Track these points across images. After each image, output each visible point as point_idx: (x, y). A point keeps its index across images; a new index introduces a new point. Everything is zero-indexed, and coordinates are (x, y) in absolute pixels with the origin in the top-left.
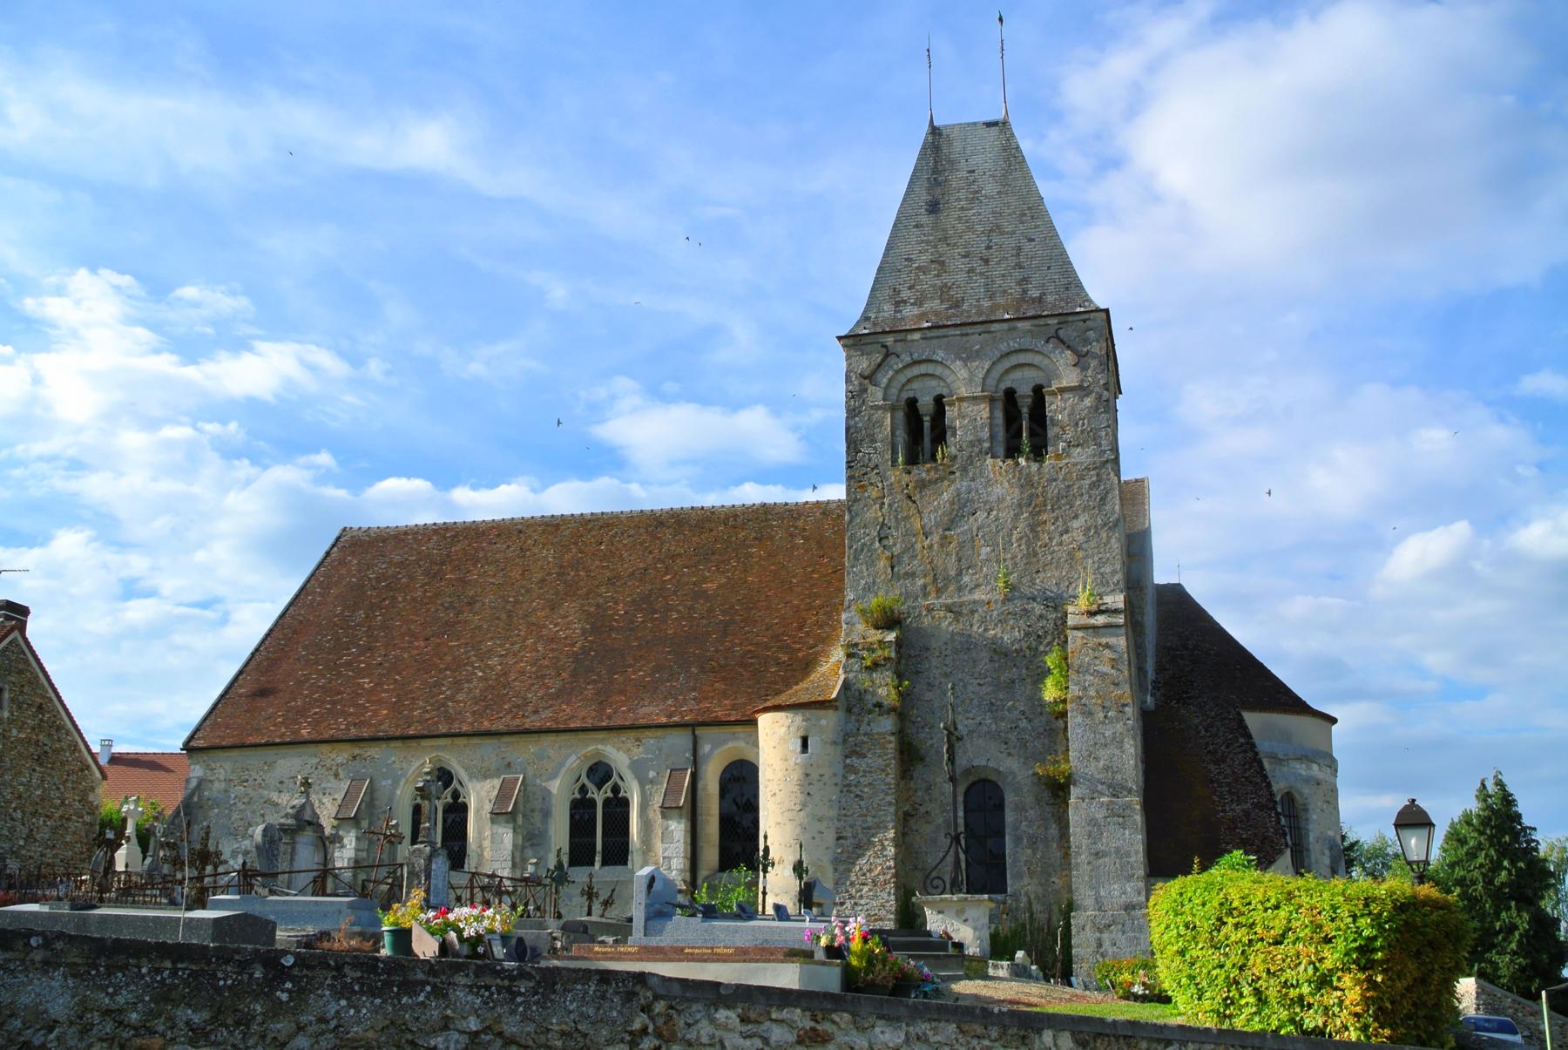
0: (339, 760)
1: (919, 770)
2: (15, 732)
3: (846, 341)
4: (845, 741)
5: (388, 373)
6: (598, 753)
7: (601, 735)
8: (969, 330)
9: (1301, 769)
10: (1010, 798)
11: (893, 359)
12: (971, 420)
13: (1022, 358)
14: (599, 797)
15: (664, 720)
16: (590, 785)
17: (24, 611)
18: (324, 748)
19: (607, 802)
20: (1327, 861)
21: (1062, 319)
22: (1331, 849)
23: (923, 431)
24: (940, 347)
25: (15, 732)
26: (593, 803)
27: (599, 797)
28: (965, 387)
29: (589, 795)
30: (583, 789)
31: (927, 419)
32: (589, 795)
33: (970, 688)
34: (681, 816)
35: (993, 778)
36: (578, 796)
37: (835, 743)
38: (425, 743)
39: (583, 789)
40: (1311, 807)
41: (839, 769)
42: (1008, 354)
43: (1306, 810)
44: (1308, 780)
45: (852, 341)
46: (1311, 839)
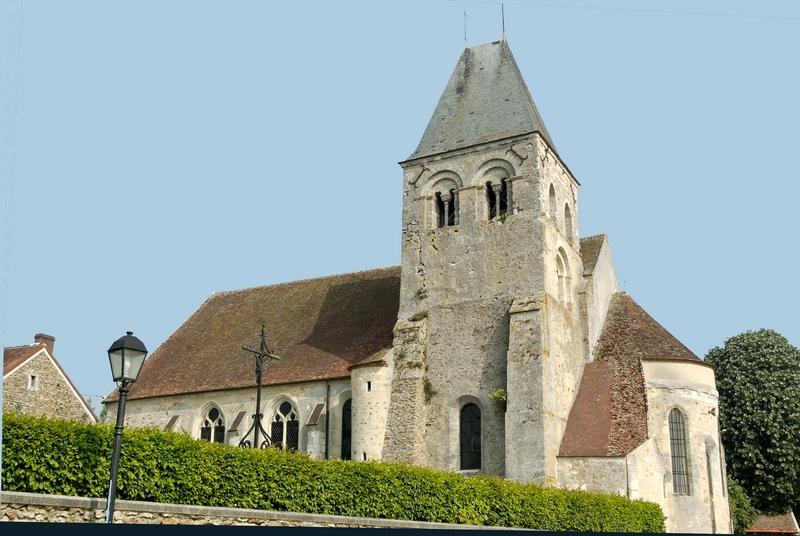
1: (434, 399)
2: (42, 398)
3: (404, 165)
6: (284, 397)
7: (284, 388)
9: (683, 394)
10: (484, 414)
11: (426, 173)
12: (473, 204)
13: (451, 176)
14: (285, 420)
15: (314, 378)
17: (52, 339)
18: (162, 400)
19: (288, 423)
21: (514, 139)
23: (447, 210)
25: (42, 398)
27: (285, 420)
28: (476, 176)
31: (446, 203)
34: (317, 429)
35: (475, 402)
38: (206, 395)
39: (278, 417)
42: (487, 162)
44: (688, 401)
45: (407, 164)
46: (691, 436)
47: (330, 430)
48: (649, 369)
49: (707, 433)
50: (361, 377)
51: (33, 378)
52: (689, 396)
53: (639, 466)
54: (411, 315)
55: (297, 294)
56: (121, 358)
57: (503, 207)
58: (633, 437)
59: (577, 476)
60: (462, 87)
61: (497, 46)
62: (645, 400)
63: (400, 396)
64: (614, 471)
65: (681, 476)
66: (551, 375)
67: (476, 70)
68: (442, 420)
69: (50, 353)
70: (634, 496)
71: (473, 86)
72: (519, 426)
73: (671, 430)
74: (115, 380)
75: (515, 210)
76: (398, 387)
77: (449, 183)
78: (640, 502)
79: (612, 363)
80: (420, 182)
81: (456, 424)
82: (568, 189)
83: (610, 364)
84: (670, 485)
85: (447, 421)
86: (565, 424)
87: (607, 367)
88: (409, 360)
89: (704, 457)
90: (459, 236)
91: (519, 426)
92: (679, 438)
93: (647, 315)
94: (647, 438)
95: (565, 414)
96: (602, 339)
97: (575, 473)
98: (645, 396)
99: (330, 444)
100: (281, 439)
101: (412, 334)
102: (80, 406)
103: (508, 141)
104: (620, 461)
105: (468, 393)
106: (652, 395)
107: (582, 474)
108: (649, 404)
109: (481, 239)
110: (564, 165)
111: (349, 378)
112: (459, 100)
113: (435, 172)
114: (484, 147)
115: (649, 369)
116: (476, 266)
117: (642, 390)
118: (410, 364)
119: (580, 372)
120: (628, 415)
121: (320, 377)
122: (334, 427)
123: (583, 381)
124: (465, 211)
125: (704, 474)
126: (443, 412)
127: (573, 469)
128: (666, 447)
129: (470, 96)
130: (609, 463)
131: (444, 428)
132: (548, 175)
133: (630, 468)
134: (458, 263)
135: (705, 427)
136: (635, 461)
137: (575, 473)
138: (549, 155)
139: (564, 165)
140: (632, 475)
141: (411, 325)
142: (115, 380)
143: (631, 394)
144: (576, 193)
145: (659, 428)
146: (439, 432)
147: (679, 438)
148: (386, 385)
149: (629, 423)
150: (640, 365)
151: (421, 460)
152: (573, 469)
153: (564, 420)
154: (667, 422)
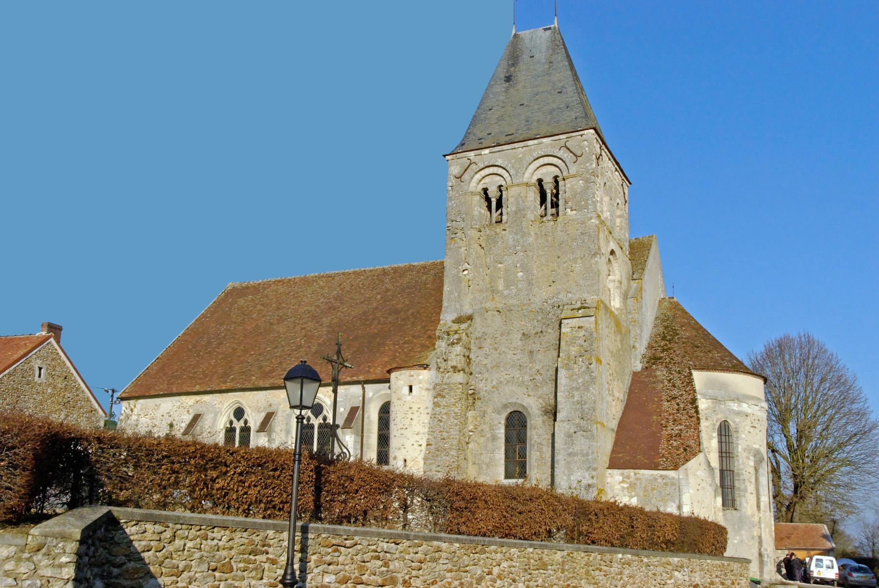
0: (190, 403)
4: (434, 388)
5: (617, 309)
8: (516, 145)
9: (734, 406)
14: (238, 425)
15: (349, 379)
16: (235, 420)
19: (320, 426)
20: (752, 463)
22: (755, 456)
24: (500, 157)
26: (312, 427)
27: (238, 425)
29: (311, 422)
30: (231, 423)
32: (311, 422)
33: (509, 356)
36: (229, 426)
37: (428, 389)
39: (231, 423)
40: (740, 430)
41: (430, 405)
43: (737, 432)
44: (738, 413)
47: (365, 434)
48: (699, 377)
49: (756, 446)
50: (400, 379)
51: (40, 369)
52: (740, 409)
53: (691, 480)
54: (454, 316)
55: (322, 288)
56: (299, 386)
57: (555, 205)
58: (685, 450)
59: (628, 488)
60: (511, 76)
61: (548, 33)
62: (697, 412)
63: (443, 402)
64: (666, 484)
65: (727, 487)
66: (602, 384)
67: (526, 57)
68: (486, 427)
69: (58, 342)
70: (686, 511)
71: (522, 74)
72: (569, 436)
73: (720, 442)
74: (292, 407)
75: (569, 210)
76: (439, 392)
77: (498, 178)
78: (650, 512)
79: (661, 373)
80: (466, 177)
81: (501, 432)
82: (620, 190)
83: (658, 373)
84: (719, 500)
85: (492, 428)
86: (614, 435)
87: (656, 376)
88: (454, 364)
89: (752, 471)
90: (507, 235)
91: (569, 436)
92: (726, 454)
93: (697, 323)
94: (700, 451)
95: (614, 424)
96: (650, 347)
97: (626, 486)
98: (697, 407)
99: (365, 449)
100: (312, 444)
101: (456, 336)
102: (89, 400)
103: (561, 137)
104: (671, 474)
105: (514, 401)
106: (703, 404)
107: (632, 486)
108: (700, 416)
109: (531, 239)
110: (617, 164)
111: (388, 381)
112: (507, 89)
113: (483, 166)
114: (536, 142)
115: (699, 377)
116: (524, 268)
117: (694, 401)
118: (454, 367)
119: (628, 380)
120: (679, 427)
121: (355, 378)
122: (370, 432)
123: (631, 392)
124: (514, 209)
125: (751, 488)
126: (487, 418)
127: (623, 482)
128: (715, 463)
129: (519, 86)
130: (494, 438)
131: (489, 435)
132: (602, 174)
133: (683, 482)
134: (506, 263)
135: (753, 436)
136: (687, 475)
137: (626, 486)
138: (603, 153)
139: (617, 164)
140: (684, 489)
141: (455, 327)
142: (292, 407)
143: (682, 406)
144: (626, 192)
145: (711, 443)
146: (482, 440)
147: (726, 454)
148: (428, 389)
149: (679, 435)
150: (691, 374)
151: (471, 474)
152: (623, 482)
153: (613, 430)
154: (715, 434)
